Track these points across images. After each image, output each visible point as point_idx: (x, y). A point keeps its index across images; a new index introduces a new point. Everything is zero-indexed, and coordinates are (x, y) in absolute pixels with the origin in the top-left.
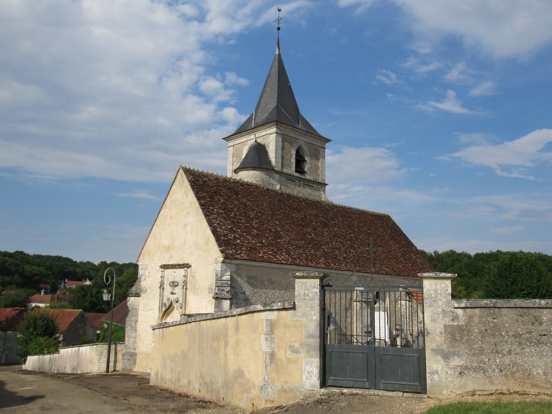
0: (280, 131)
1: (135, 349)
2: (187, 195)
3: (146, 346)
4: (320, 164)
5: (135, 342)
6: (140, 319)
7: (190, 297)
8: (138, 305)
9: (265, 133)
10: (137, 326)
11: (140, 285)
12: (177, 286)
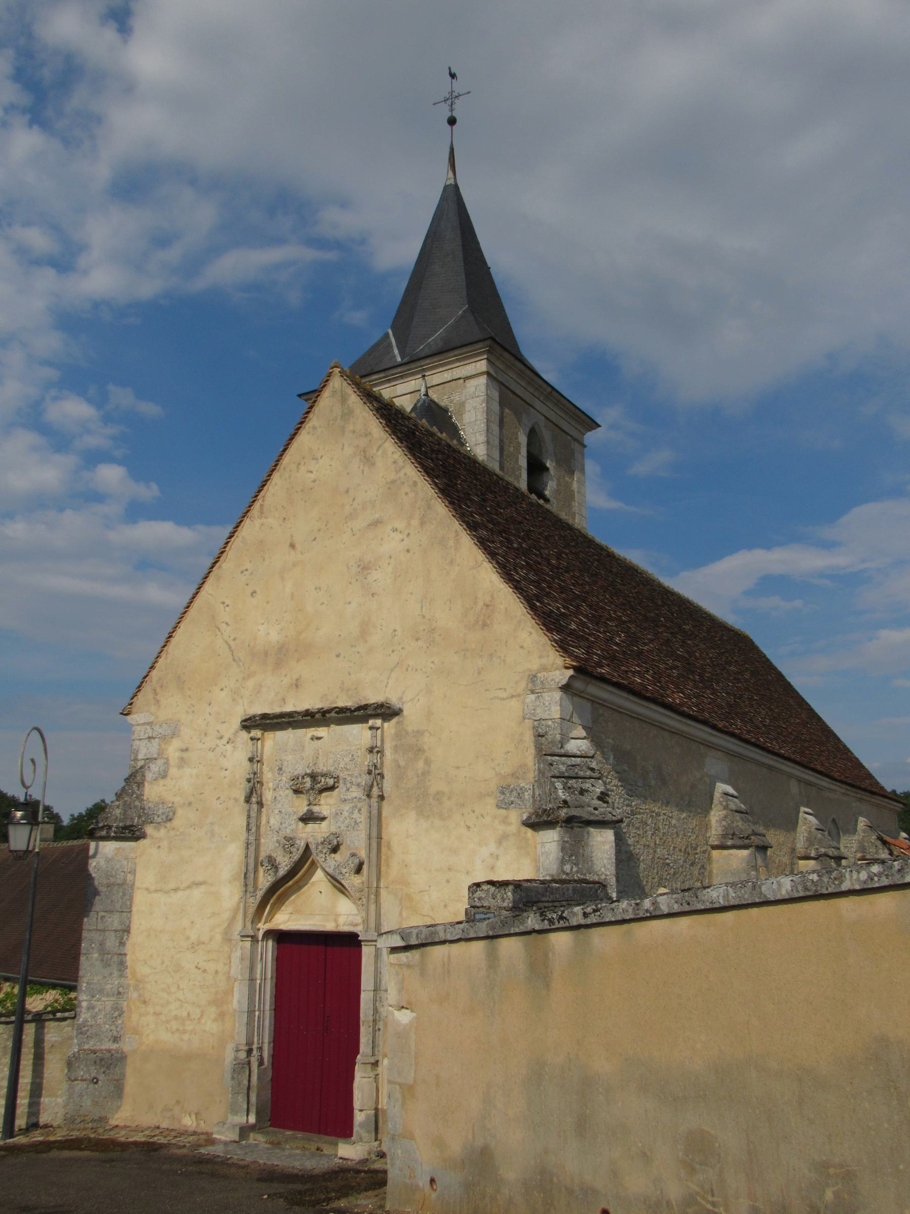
0: (496, 372)
1: (116, 1039)
2: (368, 460)
3: (174, 1025)
4: (575, 486)
5: (118, 1012)
6: (139, 923)
7: (405, 831)
8: (133, 872)
9: (447, 376)
10: (128, 949)
11: (140, 797)
12: (332, 788)
